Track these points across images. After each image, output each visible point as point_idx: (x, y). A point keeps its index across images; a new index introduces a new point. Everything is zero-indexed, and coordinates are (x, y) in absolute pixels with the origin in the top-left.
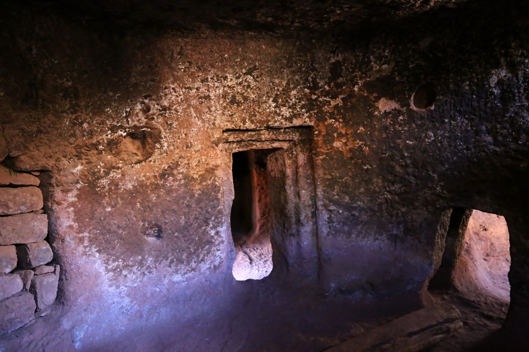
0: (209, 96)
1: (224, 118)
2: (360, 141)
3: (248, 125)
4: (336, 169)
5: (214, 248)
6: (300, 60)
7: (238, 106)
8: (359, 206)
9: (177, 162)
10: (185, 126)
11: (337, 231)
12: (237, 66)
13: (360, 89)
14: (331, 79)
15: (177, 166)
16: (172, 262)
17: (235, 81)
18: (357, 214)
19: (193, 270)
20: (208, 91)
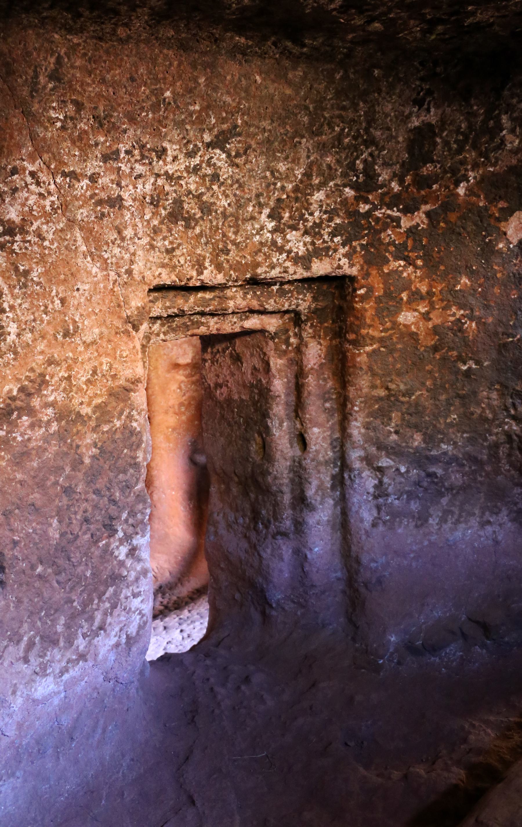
0: (120, 199)
1: (155, 257)
2: (460, 308)
3: (211, 275)
4: (399, 374)
5: (126, 592)
6: (340, 117)
7: (188, 227)
8: (445, 453)
9: (42, 375)
10: (62, 277)
11: (396, 515)
12: (193, 123)
13: (470, 191)
14: (407, 167)
15: (40, 385)
16: (31, 645)
17: (183, 163)
18: (440, 472)
19: (82, 657)
20: (119, 185)
